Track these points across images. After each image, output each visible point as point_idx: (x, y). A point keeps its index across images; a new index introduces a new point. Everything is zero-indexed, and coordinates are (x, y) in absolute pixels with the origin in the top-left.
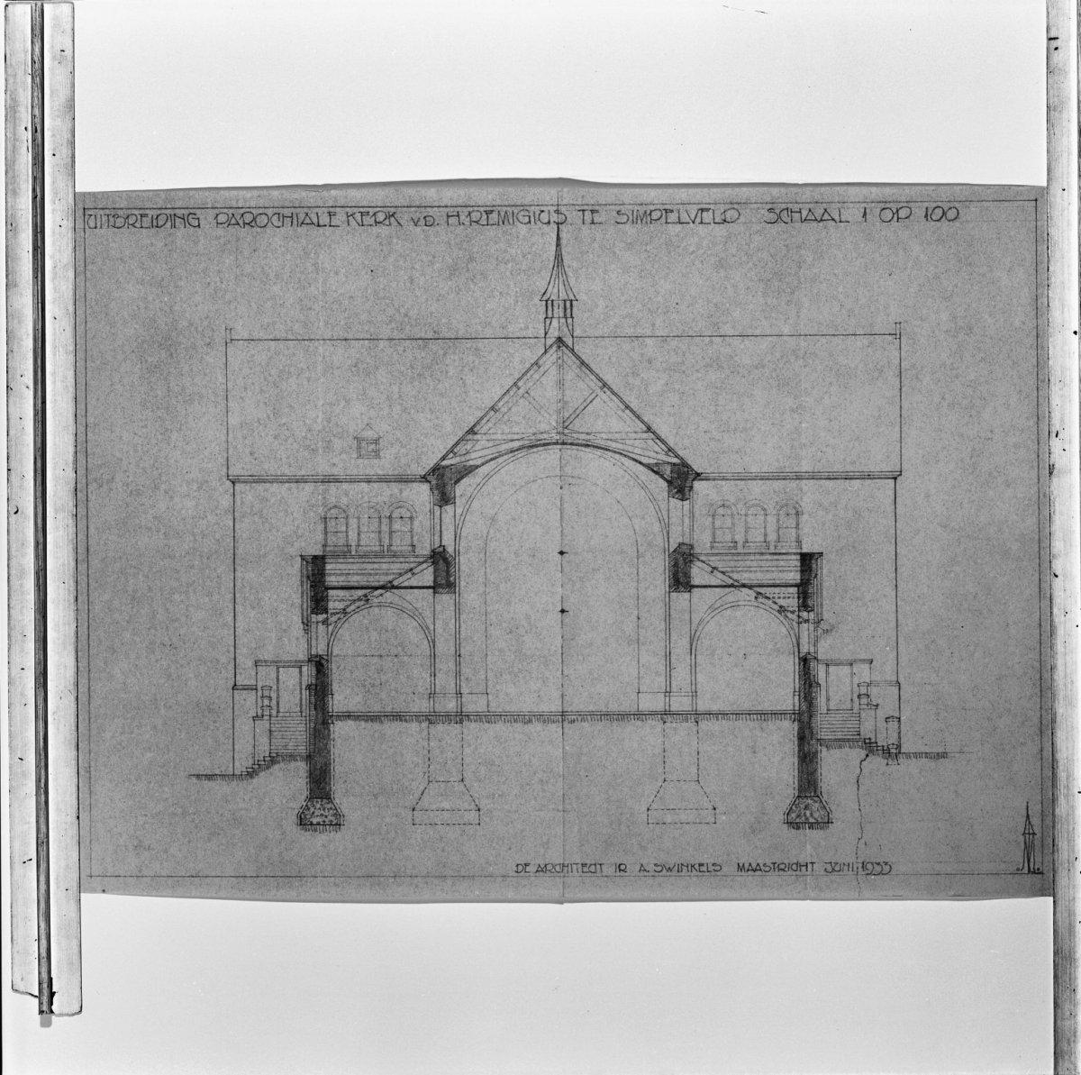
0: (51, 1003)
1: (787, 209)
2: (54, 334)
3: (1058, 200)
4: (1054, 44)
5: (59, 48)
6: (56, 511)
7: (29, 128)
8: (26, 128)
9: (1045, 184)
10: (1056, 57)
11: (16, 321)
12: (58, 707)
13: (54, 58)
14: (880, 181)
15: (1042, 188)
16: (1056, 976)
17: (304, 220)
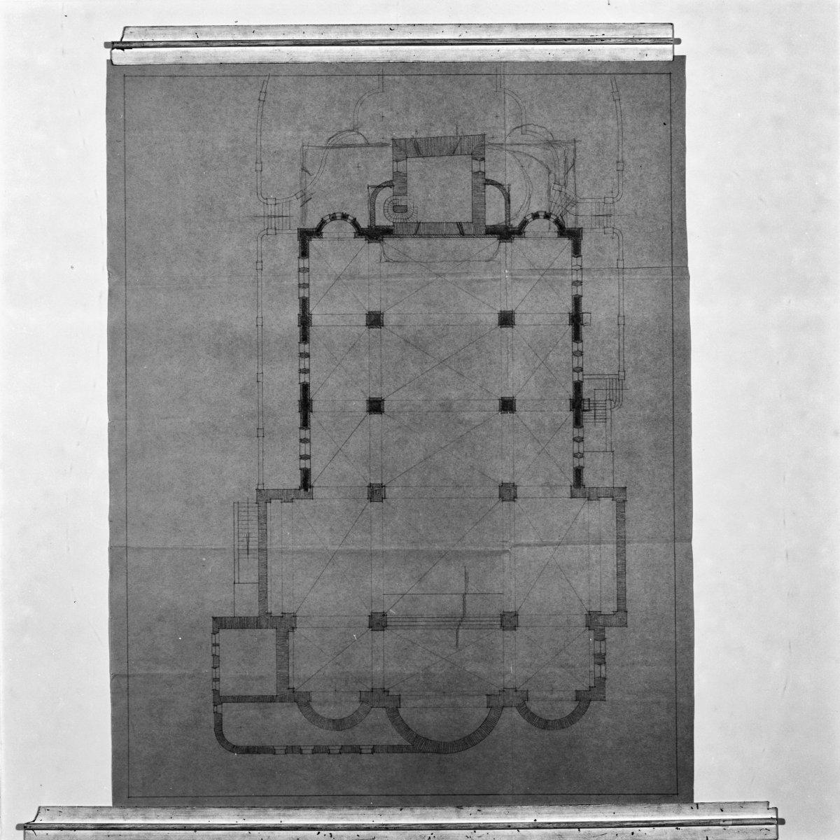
0: (118, 48)
5: (649, 53)
7: (604, 37)
13: (644, 50)
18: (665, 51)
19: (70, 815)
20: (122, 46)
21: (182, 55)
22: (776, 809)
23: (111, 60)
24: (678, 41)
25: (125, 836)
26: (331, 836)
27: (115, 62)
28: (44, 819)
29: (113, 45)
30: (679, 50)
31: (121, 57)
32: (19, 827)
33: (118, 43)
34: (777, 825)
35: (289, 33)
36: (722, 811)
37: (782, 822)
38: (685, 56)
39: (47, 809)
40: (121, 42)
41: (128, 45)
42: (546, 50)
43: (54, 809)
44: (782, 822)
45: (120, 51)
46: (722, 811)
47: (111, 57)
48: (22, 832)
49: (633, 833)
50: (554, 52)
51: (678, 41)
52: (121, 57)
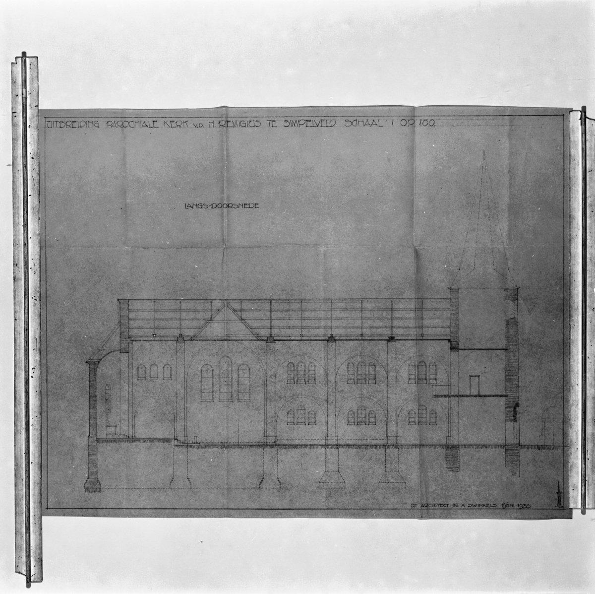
0: (581, 115)
2: (578, 379)
4: (15, 114)
5: (575, 491)
7: (587, 459)
10: (17, 315)
12: (577, 232)
13: (577, 488)
16: (15, 474)
17: (430, 420)
18: (576, 503)
19: (21, 551)
20: (584, 119)
21: (576, 161)
22: (16, 58)
23: (573, 111)
24: (584, 513)
25: (35, 512)
26: (34, 368)
27: (572, 113)
28: (24, 569)
29: (584, 110)
30: (576, 513)
31: (575, 118)
32: (28, 586)
33: (585, 115)
34: (26, 57)
35: (592, 237)
36: (17, 95)
37: (24, 54)
38: (572, 518)
39: (17, 567)
40: (586, 117)
41: (583, 123)
42: (578, 418)
43: (17, 562)
44: (24, 54)
45: (579, 117)
46: (17, 95)
47: (575, 111)
48: (32, 584)
49: (33, 158)
50: (576, 424)
51: (584, 513)
52: (575, 118)
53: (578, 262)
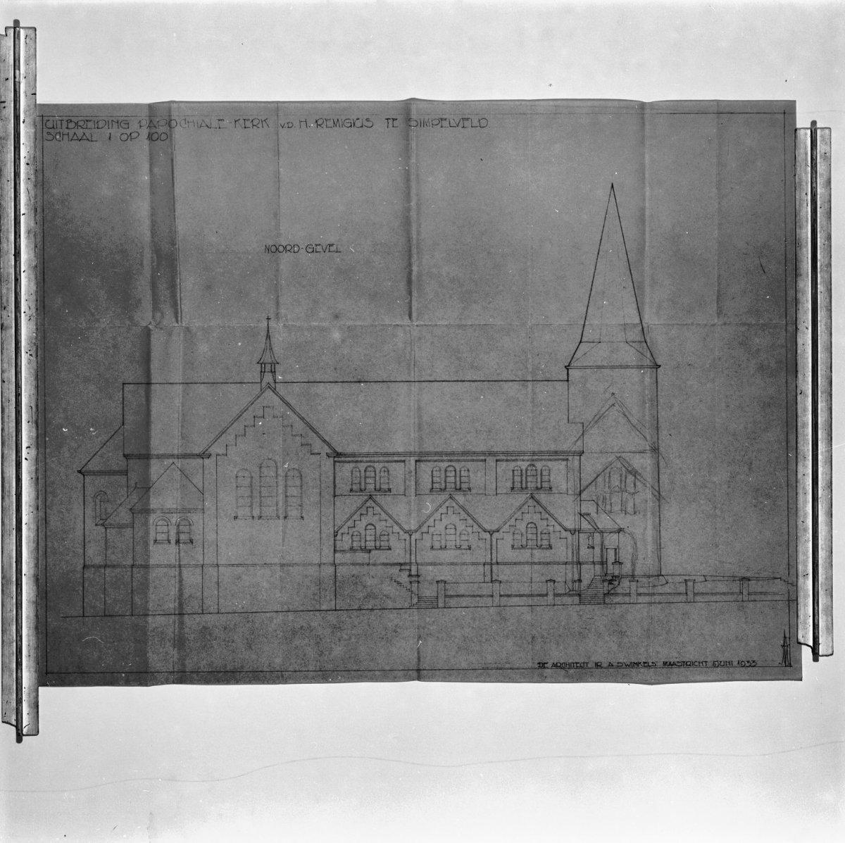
1: (185, 120)
3: (5, 186)
5: (823, 151)
6: (822, 393)
8: (806, 194)
9: (41, 689)
11: (801, 294)
14: (595, 98)
15: (45, 685)
18: (822, 136)
36: (7, 79)
46: (7, 79)
50: (823, 241)
53: (822, 455)
